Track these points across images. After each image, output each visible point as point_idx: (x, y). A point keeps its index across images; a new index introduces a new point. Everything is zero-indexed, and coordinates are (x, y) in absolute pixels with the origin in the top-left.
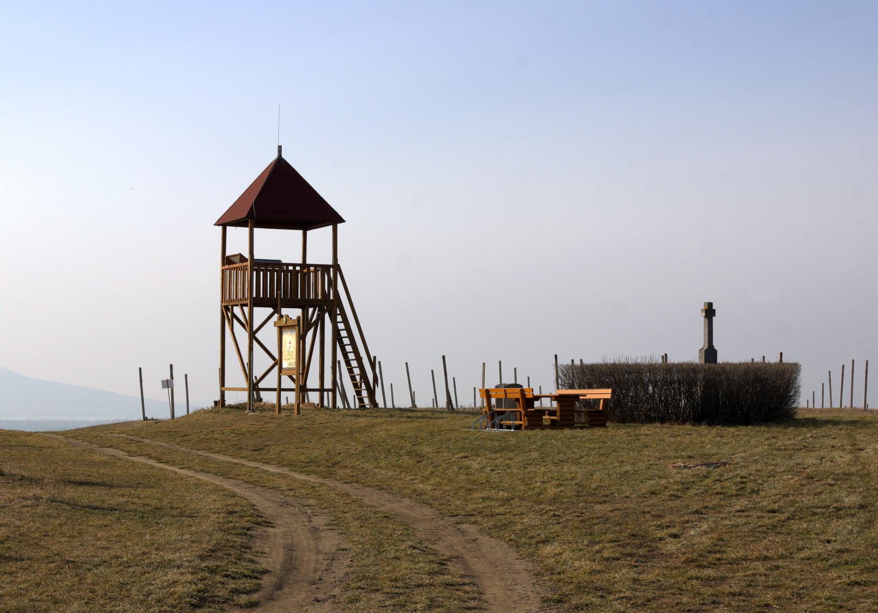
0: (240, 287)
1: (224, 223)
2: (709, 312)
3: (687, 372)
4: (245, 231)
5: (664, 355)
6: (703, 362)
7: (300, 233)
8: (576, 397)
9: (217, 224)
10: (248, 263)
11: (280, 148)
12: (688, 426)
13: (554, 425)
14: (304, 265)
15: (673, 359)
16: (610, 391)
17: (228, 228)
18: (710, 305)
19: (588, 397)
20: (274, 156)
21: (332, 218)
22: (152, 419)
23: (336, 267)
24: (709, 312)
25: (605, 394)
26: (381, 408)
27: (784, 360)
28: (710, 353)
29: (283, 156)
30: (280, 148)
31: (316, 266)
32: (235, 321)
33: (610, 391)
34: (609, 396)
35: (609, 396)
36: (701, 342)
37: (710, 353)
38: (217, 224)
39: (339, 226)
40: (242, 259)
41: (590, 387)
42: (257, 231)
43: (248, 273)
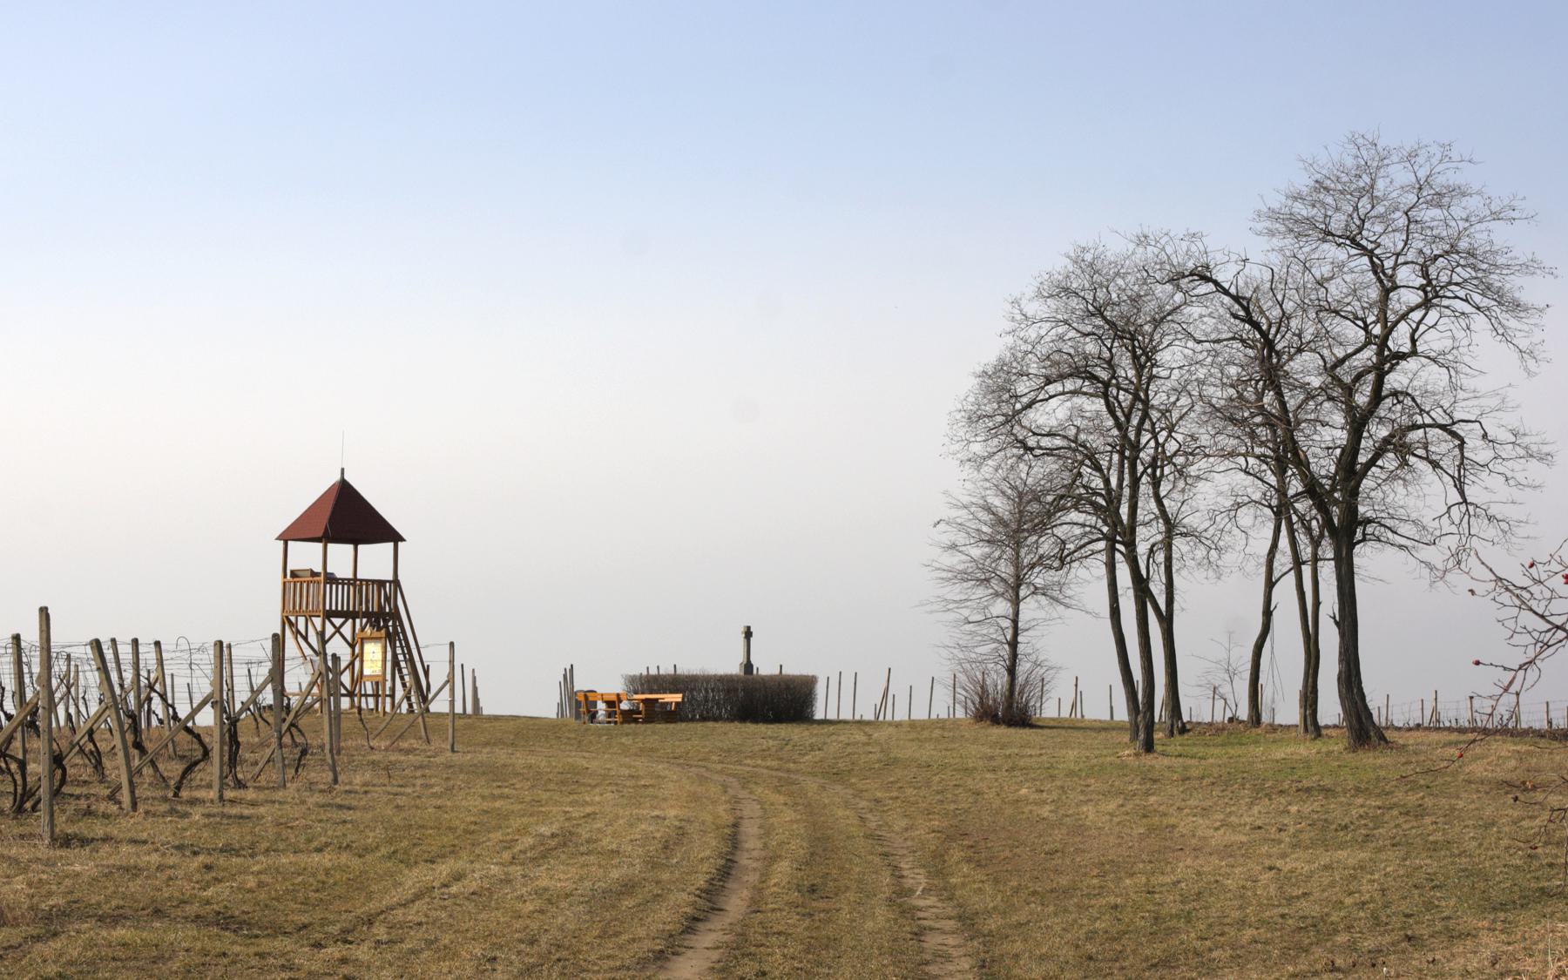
0: (311, 599)
1: (286, 537)
2: (748, 634)
3: (726, 682)
4: (320, 546)
5: (568, 667)
6: (742, 674)
7: (350, 547)
8: (657, 699)
9: (279, 538)
10: (322, 578)
11: (343, 470)
12: (736, 723)
13: (642, 723)
14: (355, 579)
15: (787, 671)
16: (681, 695)
17: (289, 542)
18: (749, 628)
19: (666, 700)
20: (337, 478)
21: (394, 537)
22: (581, 705)
23: (396, 582)
24: (748, 634)
25: (678, 698)
26: (683, 699)
27: (783, 672)
28: (748, 667)
29: (346, 478)
30: (343, 470)
31: (367, 581)
32: (349, 639)
33: (681, 695)
34: (680, 700)
35: (680, 700)
36: (741, 658)
37: (748, 667)
38: (279, 538)
39: (400, 544)
40: (314, 574)
41: (665, 693)
42: (330, 546)
43: (322, 585)
